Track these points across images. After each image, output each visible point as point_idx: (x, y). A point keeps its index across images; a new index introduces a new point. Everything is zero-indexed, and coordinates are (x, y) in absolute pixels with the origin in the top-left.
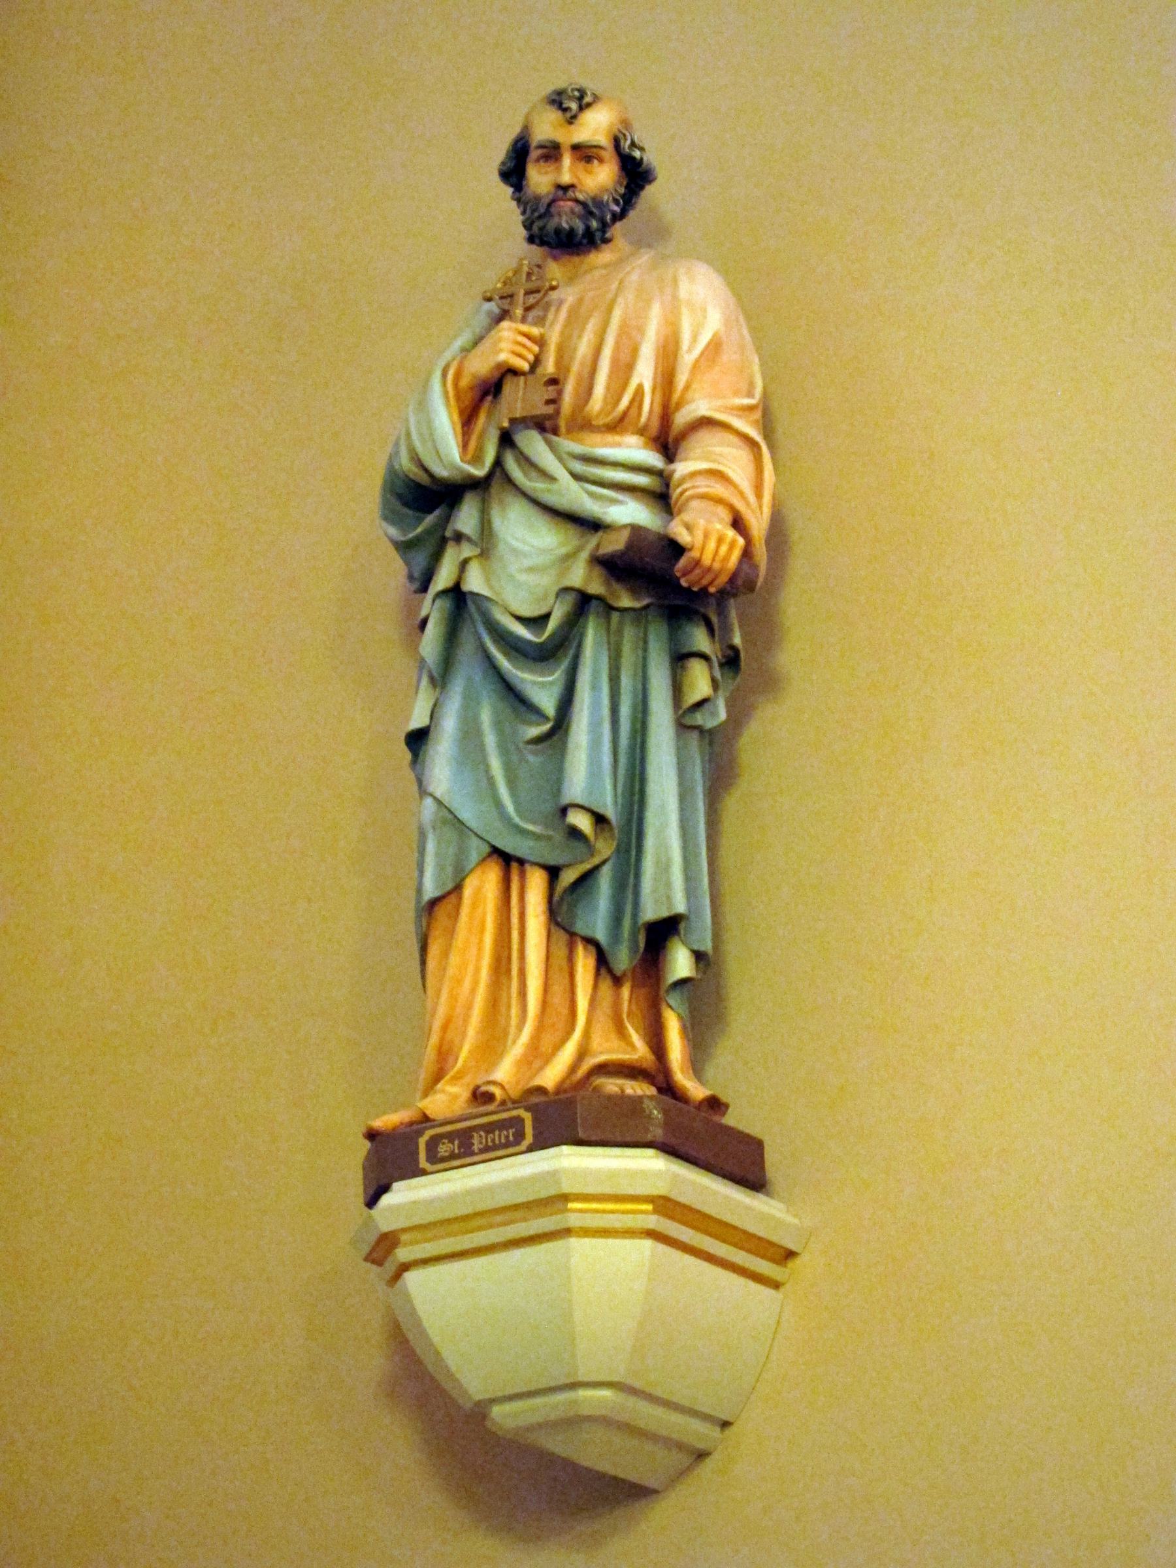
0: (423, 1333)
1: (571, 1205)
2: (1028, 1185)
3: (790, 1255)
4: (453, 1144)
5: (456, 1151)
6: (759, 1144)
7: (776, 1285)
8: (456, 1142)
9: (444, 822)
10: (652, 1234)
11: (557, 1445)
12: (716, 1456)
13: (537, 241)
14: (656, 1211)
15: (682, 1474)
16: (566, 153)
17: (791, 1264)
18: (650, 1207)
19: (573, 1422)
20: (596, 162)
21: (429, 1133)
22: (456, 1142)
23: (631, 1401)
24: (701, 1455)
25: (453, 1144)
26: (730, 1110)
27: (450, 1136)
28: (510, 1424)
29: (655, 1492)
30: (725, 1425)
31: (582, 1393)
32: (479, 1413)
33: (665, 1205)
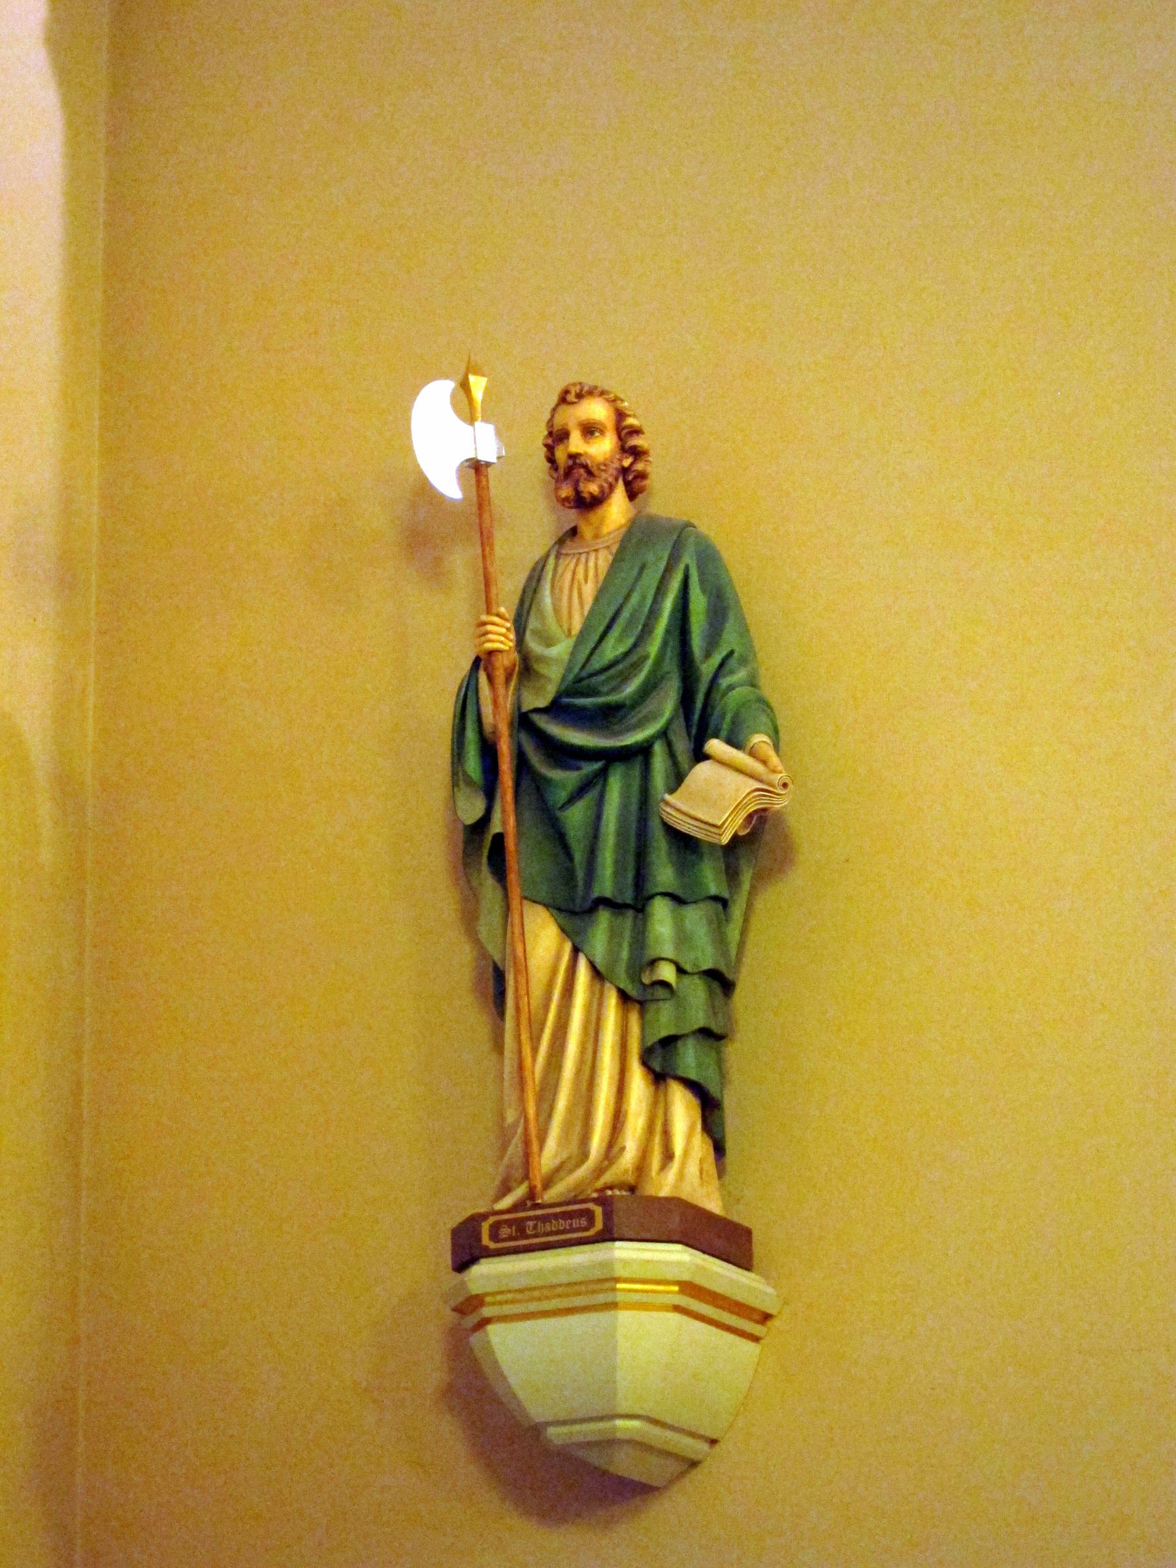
0: (503, 1377)
1: (619, 1286)
2: (404, 730)
3: (766, 1317)
4: (511, 1229)
5: (514, 1234)
6: (748, 1233)
7: (756, 1339)
8: (514, 1228)
9: (541, 1021)
10: (677, 1309)
11: (595, 1458)
12: (706, 1464)
13: (637, 608)
14: (681, 1292)
15: (682, 1474)
16: (575, 431)
17: (769, 1323)
18: (676, 1288)
19: (610, 1443)
20: (597, 434)
21: (492, 1220)
22: (514, 1228)
23: (657, 1431)
24: (694, 1464)
25: (511, 1229)
26: (757, 1237)
27: (509, 1223)
28: (558, 1442)
29: (657, 1489)
30: (713, 1442)
31: (620, 1423)
32: (537, 1430)
33: (690, 1288)
